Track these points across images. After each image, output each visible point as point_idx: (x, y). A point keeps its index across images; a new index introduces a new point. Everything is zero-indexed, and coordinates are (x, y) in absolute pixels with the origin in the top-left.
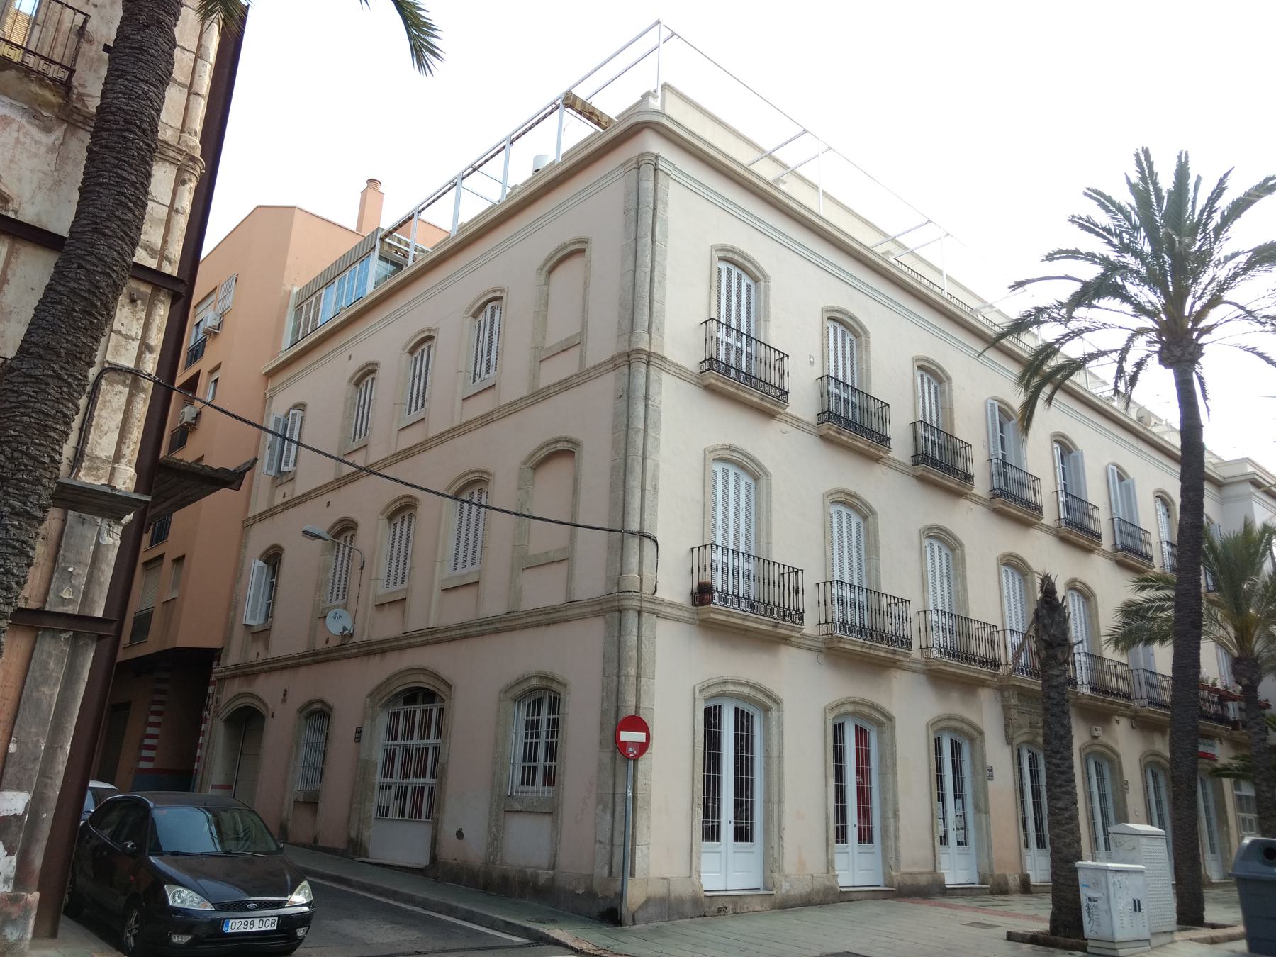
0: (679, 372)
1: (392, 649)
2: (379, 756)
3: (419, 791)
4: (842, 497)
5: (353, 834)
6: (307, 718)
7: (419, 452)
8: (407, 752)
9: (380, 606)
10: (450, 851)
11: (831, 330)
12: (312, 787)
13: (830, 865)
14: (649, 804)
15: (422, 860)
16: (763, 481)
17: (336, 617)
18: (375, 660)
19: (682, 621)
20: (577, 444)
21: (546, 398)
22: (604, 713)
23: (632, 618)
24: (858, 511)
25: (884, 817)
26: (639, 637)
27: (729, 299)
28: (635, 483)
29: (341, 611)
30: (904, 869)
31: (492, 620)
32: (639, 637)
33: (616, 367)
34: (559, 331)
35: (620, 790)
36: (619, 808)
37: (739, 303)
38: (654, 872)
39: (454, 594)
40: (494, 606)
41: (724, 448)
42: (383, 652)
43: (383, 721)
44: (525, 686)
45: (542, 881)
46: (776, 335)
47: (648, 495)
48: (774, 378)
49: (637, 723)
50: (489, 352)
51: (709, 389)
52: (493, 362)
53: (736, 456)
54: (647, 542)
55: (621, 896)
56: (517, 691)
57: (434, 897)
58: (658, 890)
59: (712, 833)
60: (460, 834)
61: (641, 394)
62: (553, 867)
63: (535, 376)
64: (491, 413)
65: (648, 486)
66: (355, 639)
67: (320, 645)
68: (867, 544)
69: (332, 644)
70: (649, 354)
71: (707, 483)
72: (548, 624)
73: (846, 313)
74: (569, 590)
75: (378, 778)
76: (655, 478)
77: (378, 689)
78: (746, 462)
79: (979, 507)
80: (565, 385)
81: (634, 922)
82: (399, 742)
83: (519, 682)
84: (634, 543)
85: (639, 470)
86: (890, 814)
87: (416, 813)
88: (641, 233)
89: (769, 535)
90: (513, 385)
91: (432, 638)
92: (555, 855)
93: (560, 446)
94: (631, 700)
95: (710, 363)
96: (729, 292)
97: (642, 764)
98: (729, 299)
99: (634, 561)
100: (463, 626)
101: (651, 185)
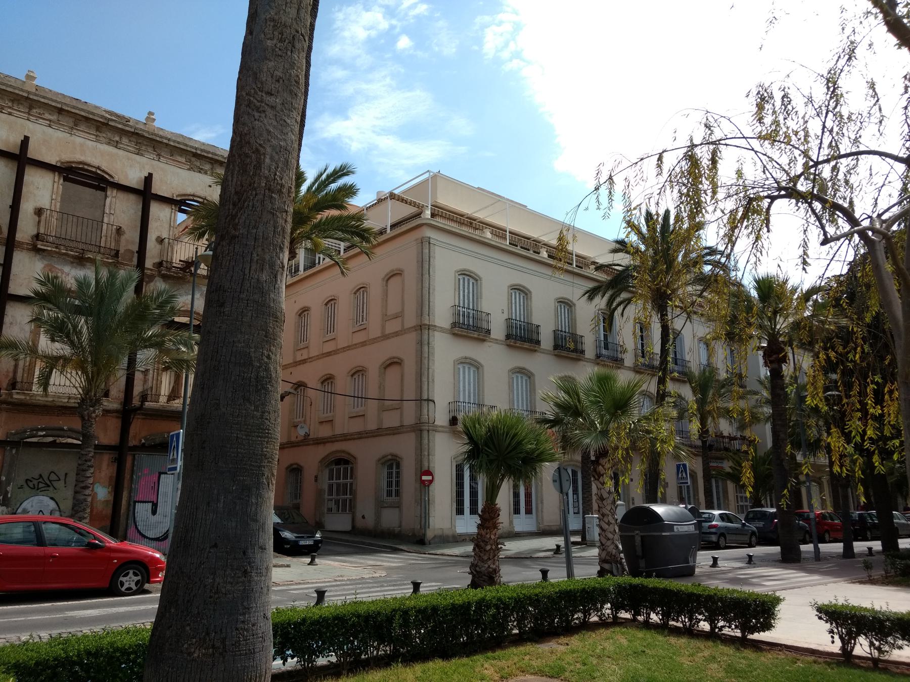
0: (442, 330)
1: (329, 442)
2: (326, 487)
3: (345, 501)
4: (518, 370)
5: (318, 520)
6: (290, 471)
7: (334, 354)
8: (338, 485)
9: (321, 423)
10: (360, 523)
11: (513, 294)
12: (295, 502)
13: (511, 522)
14: (434, 502)
15: (348, 527)
16: (480, 370)
17: (302, 427)
18: (321, 447)
19: (446, 432)
20: (402, 360)
21: (389, 338)
22: (416, 469)
23: (425, 434)
24: (526, 375)
25: (537, 504)
26: (428, 440)
27: (464, 291)
28: (425, 379)
29: (303, 425)
30: (545, 524)
31: (372, 432)
32: (428, 440)
33: (416, 330)
34: (393, 309)
35: (423, 497)
36: (423, 504)
37: (469, 292)
38: (437, 526)
39: (327, 343)
40: (372, 426)
41: (462, 358)
42: (324, 443)
43: (327, 472)
44: (386, 459)
45: (396, 532)
46: (485, 306)
47: (430, 384)
48: (485, 326)
49: (428, 473)
50: (363, 312)
51: (454, 334)
52: (365, 316)
53: (468, 361)
54: (431, 404)
55: (424, 535)
56: (383, 460)
57: (356, 539)
58: (439, 533)
59: (460, 511)
60: (363, 517)
61: (426, 342)
62: (400, 526)
63: (383, 327)
64: (365, 341)
65: (430, 380)
66: (311, 437)
67: (293, 439)
68: (530, 388)
69: (299, 439)
70: (429, 325)
71: (456, 374)
72: (394, 434)
73: (520, 285)
74: (401, 421)
75: (326, 496)
76: (433, 376)
77: (324, 459)
78: (473, 362)
79: (589, 364)
80: (396, 334)
81: (430, 544)
82: (334, 481)
83: (383, 457)
84: (425, 404)
85: (426, 374)
86: (539, 502)
87: (344, 510)
88: (424, 272)
89: (483, 392)
90: (374, 331)
91: (346, 437)
92: (401, 522)
93: (395, 360)
94: (426, 464)
95: (454, 325)
96: (464, 288)
97: (431, 488)
98: (464, 291)
99: (425, 411)
100: (359, 433)
101: (427, 251)
